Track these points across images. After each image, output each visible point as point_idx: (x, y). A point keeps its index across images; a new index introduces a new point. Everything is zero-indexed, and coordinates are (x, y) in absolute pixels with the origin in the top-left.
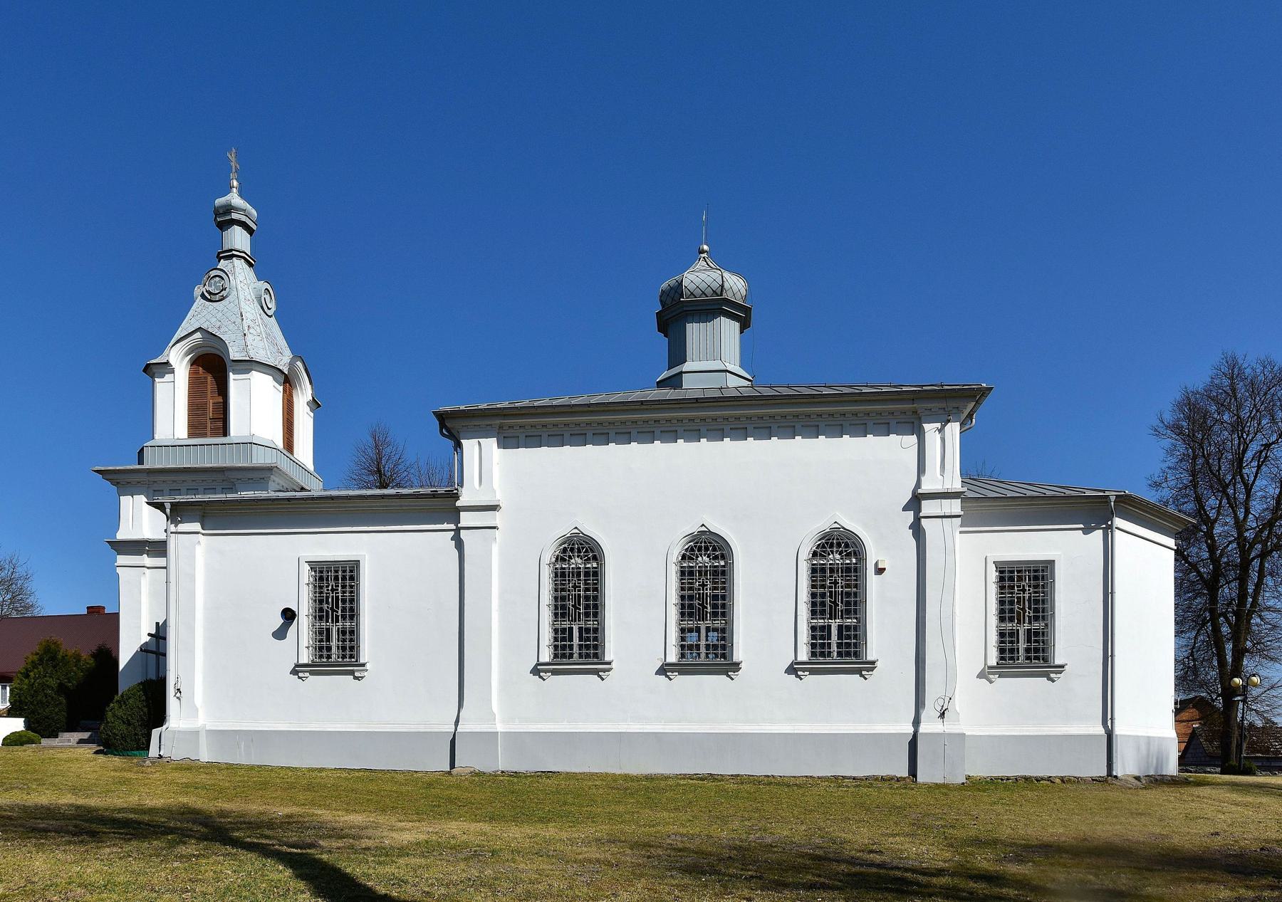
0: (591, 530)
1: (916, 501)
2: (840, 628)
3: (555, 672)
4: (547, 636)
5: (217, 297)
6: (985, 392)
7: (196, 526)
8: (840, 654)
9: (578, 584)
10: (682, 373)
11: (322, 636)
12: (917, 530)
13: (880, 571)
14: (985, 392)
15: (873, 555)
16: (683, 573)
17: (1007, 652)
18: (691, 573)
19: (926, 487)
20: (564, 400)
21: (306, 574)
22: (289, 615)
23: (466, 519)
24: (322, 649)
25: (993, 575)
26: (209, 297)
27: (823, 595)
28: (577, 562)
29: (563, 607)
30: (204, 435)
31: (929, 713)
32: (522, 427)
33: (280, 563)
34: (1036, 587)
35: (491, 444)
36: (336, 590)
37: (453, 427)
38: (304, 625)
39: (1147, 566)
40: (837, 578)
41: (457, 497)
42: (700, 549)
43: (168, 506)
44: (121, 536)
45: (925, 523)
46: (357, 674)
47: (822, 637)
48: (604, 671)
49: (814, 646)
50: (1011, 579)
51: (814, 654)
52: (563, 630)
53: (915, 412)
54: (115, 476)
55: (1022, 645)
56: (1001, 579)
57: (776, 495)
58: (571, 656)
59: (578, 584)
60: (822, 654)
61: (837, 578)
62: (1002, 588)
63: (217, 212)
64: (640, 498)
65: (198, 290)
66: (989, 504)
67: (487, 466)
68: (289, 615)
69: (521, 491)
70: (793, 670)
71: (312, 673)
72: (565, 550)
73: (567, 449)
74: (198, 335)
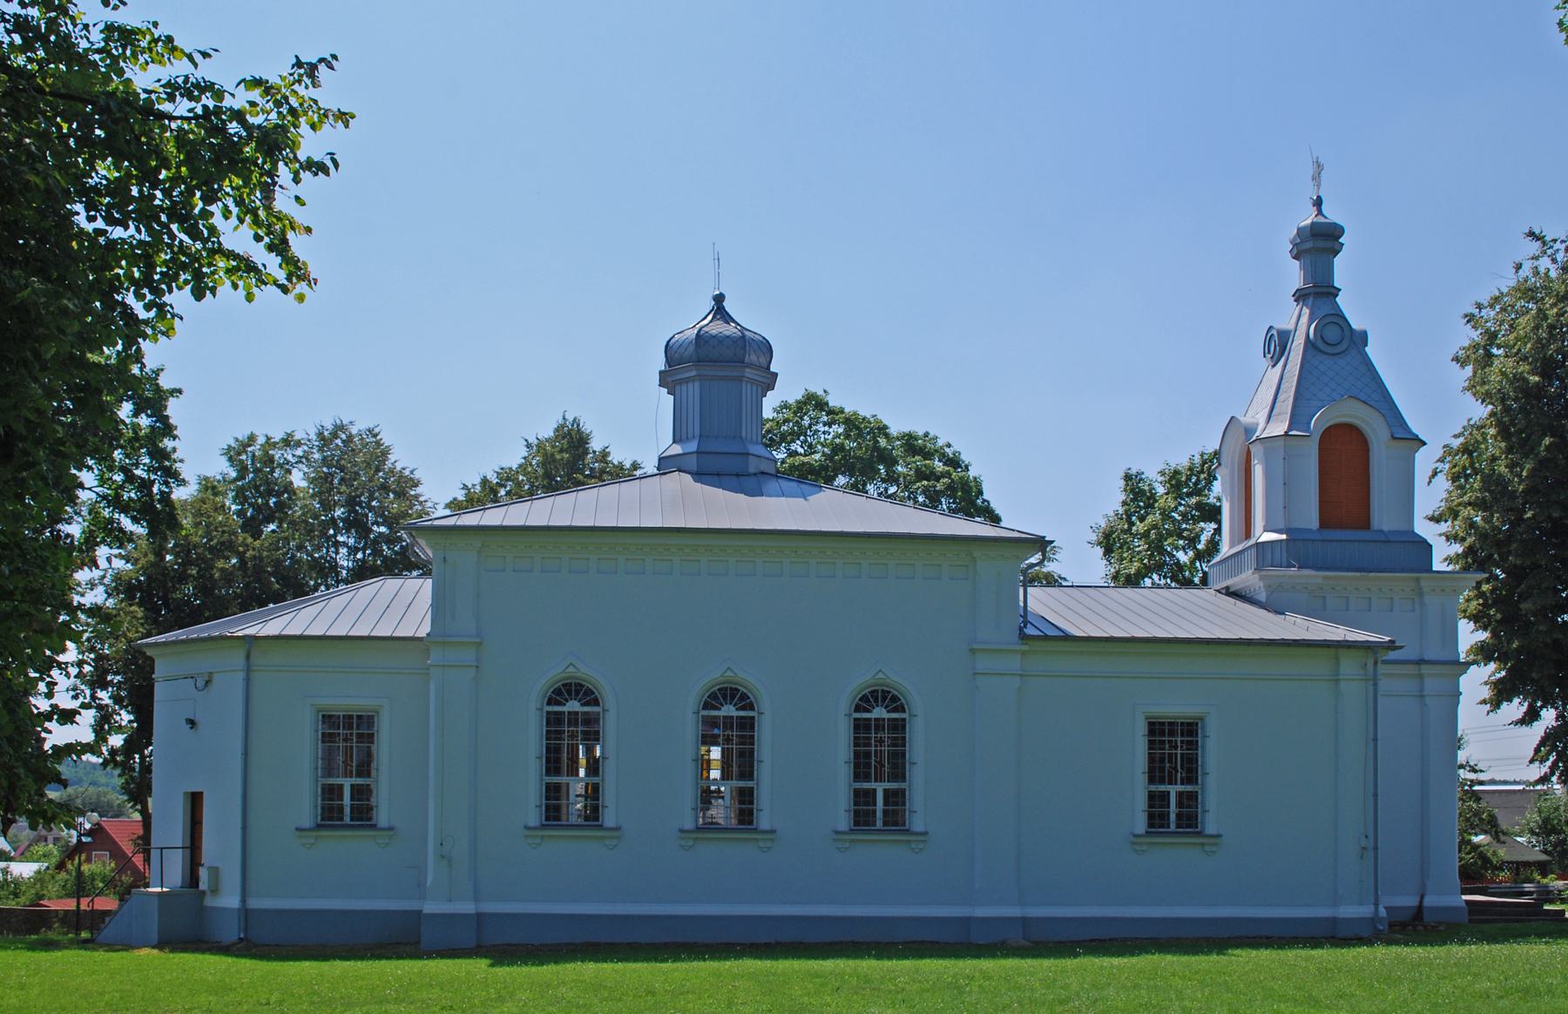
2: (886, 791)
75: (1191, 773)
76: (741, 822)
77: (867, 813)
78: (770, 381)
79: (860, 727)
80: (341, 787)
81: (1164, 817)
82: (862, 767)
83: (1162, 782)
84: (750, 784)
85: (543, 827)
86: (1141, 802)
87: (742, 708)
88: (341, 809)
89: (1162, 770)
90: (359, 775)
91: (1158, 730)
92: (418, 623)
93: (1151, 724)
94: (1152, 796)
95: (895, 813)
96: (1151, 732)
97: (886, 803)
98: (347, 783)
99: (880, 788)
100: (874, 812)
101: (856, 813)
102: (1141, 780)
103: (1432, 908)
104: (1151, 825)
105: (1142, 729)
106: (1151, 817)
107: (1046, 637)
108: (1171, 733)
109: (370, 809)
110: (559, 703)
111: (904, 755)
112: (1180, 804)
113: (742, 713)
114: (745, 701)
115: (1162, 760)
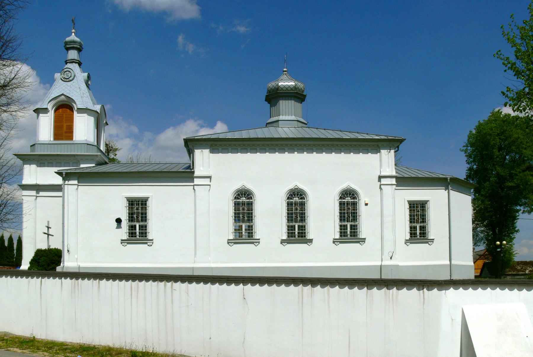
0: (250, 186)
1: (380, 178)
2: (299, 226)
3: (341, 242)
4: (338, 229)
5: (68, 80)
6: (401, 141)
7: (76, 182)
8: (351, 236)
9: (244, 207)
10: (278, 121)
11: (132, 228)
12: (380, 188)
13: (366, 204)
14: (401, 141)
15: (363, 198)
16: (235, 204)
17: (413, 234)
18: (292, 204)
19: (383, 174)
20: (245, 134)
21: (126, 203)
22: (119, 221)
23: (197, 181)
24: (132, 234)
25: (407, 206)
26: (66, 80)
27: (292, 214)
28: (244, 199)
29: (132, 217)
30: (62, 139)
31: (386, 256)
32: (217, 145)
33: (114, 198)
34: (423, 210)
35: (206, 151)
36: (138, 209)
37: (191, 145)
38: (125, 224)
39: (463, 204)
40: (348, 207)
41: (193, 172)
42: (242, 195)
43: (64, 173)
44: (24, 182)
45: (382, 186)
46: (148, 244)
47: (344, 229)
48: (256, 242)
49: (341, 233)
50: (414, 207)
51: (341, 236)
52: (292, 226)
53: (378, 146)
54: (23, 157)
55: (418, 232)
56: (410, 207)
57: (323, 175)
58: (136, 237)
59: (244, 207)
60: (344, 236)
61: (348, 207)
62: (410, 210)
63: (66, 43)
64: (270, 176)
65: (57, 76)
66: (403, 181)
67: (204, 161)
68: (119, 221)
69: (222, 172)
70: (335, 241)
71: (128, 243)
72: (239, 195)
73: (230, 154)
74: (63, 97)
75: (144, 218)
76: (249, 236)
77: (344, 232)
78: (510, 115)
79: (237, 204)
81: (415, 234)
84: (251, 224)
87: (248, 198)
88: (135, 233)
89: (414, 219)
90: (142, 221)
93: (410, 204)
94: (411, 228)
95: (302, 233)
97: (299, 230)
100: (295, 233)
101: (288, 233)
106: (411, 234)
110: (238, 199)
111: (305, 214)
112: (351, 229)
113: (301, 201)
115: (414, 216)
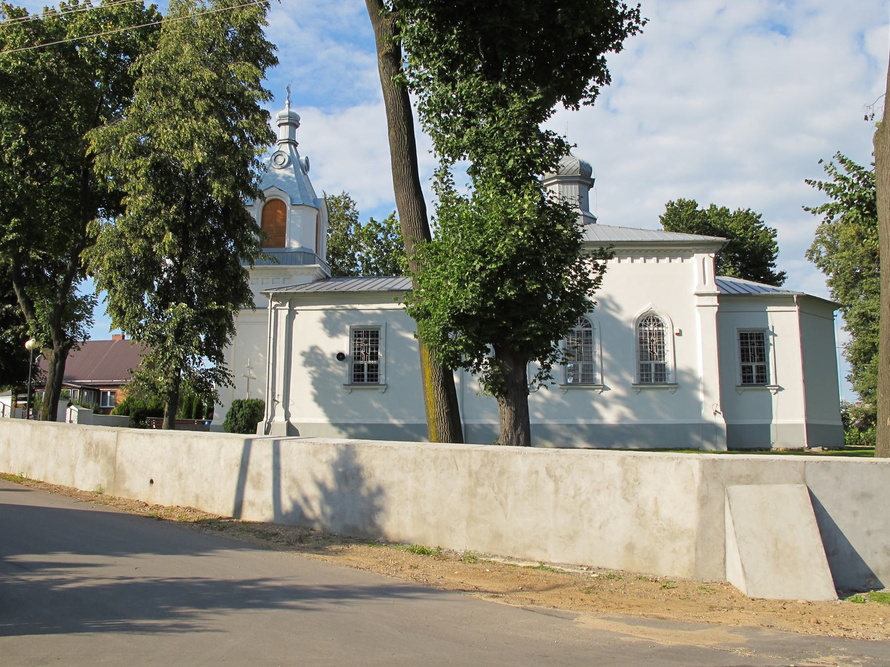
2: (757, 367)
80: (363, 365)
82: (744, 357)
83: (748, 361)
85: (742, 385)
86: (739, 371)
87: (586, 326)
88: (363, 376)
90: (372, 359)
91: (744, 337)
92: (409, 286)
94: (744, 368)
96: (742, 338)
98: (754, 365)
99: (754, 365)
102: (738, 360)
103: (535, 425)
104: (744, 382)
105: (737, 337)
106: (744, 377)
107: (741, 295)
108: (751, 338)
109: (377, 376)
114: (658, 323)
